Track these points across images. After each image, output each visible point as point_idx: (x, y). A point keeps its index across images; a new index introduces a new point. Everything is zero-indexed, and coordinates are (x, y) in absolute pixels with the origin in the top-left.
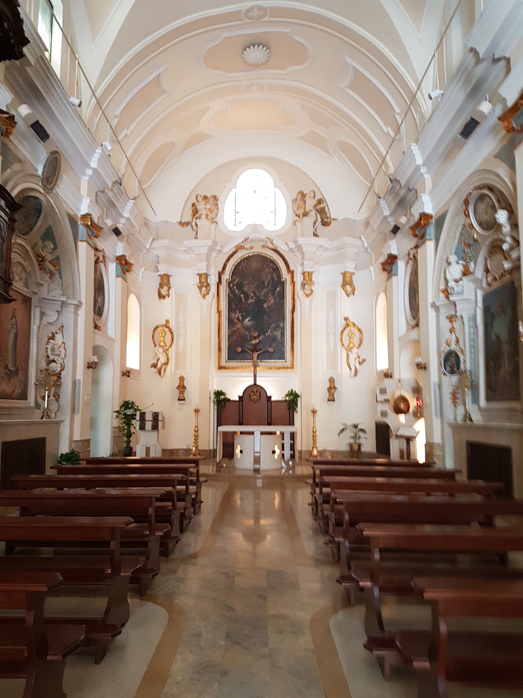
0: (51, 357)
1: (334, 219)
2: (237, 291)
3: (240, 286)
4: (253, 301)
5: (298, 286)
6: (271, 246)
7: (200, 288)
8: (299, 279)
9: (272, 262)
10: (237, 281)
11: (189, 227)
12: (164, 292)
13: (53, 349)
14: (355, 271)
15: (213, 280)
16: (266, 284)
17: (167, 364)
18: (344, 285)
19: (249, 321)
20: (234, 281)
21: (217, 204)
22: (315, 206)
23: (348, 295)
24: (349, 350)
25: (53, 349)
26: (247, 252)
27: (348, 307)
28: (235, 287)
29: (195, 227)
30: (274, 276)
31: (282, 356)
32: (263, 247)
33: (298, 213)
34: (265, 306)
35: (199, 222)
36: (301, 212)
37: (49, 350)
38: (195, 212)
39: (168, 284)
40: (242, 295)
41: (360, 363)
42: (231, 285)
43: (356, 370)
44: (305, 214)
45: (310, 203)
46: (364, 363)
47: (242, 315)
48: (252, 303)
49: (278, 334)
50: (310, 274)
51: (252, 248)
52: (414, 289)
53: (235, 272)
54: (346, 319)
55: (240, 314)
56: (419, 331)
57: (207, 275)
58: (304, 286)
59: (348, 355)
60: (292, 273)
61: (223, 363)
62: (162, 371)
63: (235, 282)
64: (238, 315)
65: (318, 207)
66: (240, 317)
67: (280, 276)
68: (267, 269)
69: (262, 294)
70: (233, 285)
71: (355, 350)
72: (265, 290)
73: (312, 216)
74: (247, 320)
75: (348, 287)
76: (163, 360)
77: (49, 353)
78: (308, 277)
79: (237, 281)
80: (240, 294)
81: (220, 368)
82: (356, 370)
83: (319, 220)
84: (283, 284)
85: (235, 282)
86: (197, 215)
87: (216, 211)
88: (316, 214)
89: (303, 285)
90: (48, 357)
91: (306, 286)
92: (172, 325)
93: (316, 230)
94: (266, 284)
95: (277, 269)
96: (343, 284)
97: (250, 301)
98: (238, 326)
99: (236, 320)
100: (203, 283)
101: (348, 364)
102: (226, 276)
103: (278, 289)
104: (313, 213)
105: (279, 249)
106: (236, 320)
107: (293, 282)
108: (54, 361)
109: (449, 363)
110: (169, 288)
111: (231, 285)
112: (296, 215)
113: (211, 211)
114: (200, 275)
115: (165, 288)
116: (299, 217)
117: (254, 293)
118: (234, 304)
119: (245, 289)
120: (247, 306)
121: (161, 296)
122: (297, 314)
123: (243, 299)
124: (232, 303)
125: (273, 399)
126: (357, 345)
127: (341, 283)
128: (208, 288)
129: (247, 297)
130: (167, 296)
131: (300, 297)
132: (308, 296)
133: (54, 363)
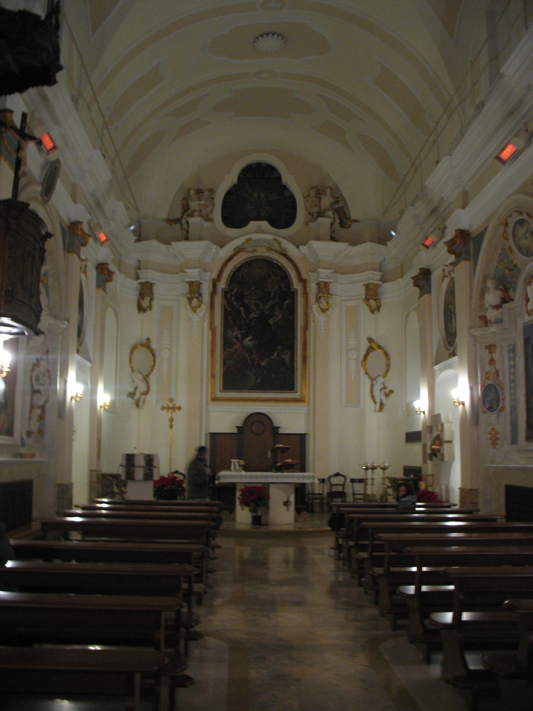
0: (36, 387)
1: (356, 221)
2: (235, 303)
3: (239, 297)
4: (256, 315)
5: (312, 298)
6: (278, 249)
7: (190, 300)
8: (312, 288)
9: (280, 268)
10: (235, 291)
11: (178, 226)
12: (145, 303)
13: (37, 378)
14: (380, 283)
15: (206, 289)
16: (272, 295)
17: (146, 393)
18: (367, 299)
19: (250, 340)
20: (232, 291)
21: (213, 199)
22: (332, 205)
23: (372, 311)
24: (373, 380)
25: (37, 378)
26: (251, 255)
27: (371, 326)
28: (233, 299)
29: (185, 226)
30: (283, 285)
31: (290, 386)
32: (270, 249)
33: (311, 211)
34: (271, 322)
35: (191, 220)
36: (315, 210)
37: (34, 379)
38: (186, 209)
39: (151, 294)
40: (242, 309)
41: (387, 395)
42: (229, 296)
43: (382, 404)
44: (321, 214)
45: (326, 201)
46: (392, 395)
47: (241, 334)
48: (254, 318)
49: (287, 357)
50: (327, 284)
51: (255, 251)
52: (450, 309)
53: (234, 278)
54: (370, 340)
55: (239, 332)
56: (170, 468)
57: (199, 284)
58: (320, 299)
59: (372, 386)
60: (304, 282)
61: (219, 395)
62: (141, 403)
63: (233, 293)
64: (237, 333)
65: (336, 206)
66: (239, 336)
67: (289, 284)
68: (273, 277)
69: (267, 307)
70: (231, 296)
71: (380, 380)
72: (271, 303)
73: (328, 217)
74: (247, 339)
75: (372, 303)
76: (142, 388)
77: (34, 382)
78: (324, 289)
79: (235, 291)
80: (239, 307)
81: (215, 399)
82: (382, 404)
83: (338, 221)
84: (293, 294)
85: (233, 293)
86: (189, 212)
87: (211, 206)
88: (334, 214)
89: (318, 299)
90: (32, 386)
91: (322, 298)
92: (154, 345)
93: (333, 231)
94: (272, 295)
95: (285, 277)
96: (366, 298)
97: (253, 315)
98: (237, 347)
99: (234, 340)
100: (194, 290)
101: (373, 397)
102: (222, 285)
103: (287, 302)
104: (330, 213)
105: (288, 254)
106: (234, 340)
107: (306, 294)
108: (38, 392)
109: (488, 399)
110: (152, 299)
111: (229, 296)
112: (310, 214)
113: (206, 207)
114: (191, 284)
115: (147, 299)
116: (313, 216)
117: (257, 305)
118: (231, 318)
119: (246, 301)
120: (248, 322)
121: (141, 309)
122: (311, 333)
123: (243, 314)
124: (230, 317)
125: (281, 431)
126: (382, 373)
127: (364, 296)
128: (200, 299)
129: (248, 313)
130: (148, 309)
131: (315, 312)
132: (324, 311)
133: (39, 395)
